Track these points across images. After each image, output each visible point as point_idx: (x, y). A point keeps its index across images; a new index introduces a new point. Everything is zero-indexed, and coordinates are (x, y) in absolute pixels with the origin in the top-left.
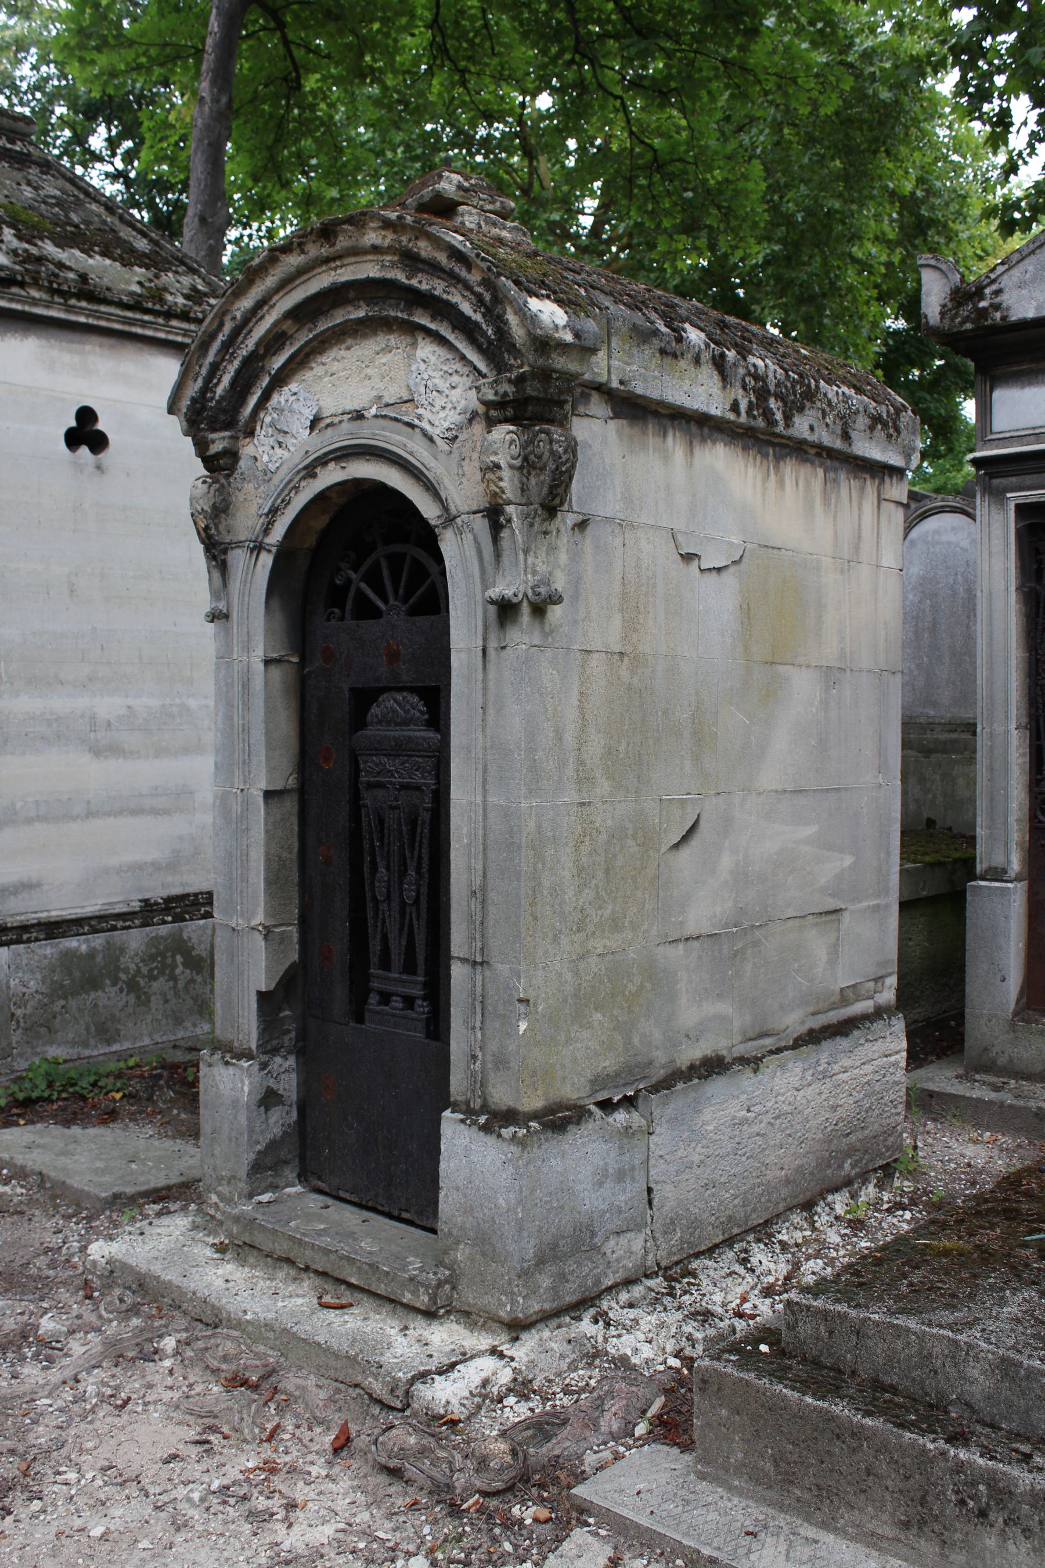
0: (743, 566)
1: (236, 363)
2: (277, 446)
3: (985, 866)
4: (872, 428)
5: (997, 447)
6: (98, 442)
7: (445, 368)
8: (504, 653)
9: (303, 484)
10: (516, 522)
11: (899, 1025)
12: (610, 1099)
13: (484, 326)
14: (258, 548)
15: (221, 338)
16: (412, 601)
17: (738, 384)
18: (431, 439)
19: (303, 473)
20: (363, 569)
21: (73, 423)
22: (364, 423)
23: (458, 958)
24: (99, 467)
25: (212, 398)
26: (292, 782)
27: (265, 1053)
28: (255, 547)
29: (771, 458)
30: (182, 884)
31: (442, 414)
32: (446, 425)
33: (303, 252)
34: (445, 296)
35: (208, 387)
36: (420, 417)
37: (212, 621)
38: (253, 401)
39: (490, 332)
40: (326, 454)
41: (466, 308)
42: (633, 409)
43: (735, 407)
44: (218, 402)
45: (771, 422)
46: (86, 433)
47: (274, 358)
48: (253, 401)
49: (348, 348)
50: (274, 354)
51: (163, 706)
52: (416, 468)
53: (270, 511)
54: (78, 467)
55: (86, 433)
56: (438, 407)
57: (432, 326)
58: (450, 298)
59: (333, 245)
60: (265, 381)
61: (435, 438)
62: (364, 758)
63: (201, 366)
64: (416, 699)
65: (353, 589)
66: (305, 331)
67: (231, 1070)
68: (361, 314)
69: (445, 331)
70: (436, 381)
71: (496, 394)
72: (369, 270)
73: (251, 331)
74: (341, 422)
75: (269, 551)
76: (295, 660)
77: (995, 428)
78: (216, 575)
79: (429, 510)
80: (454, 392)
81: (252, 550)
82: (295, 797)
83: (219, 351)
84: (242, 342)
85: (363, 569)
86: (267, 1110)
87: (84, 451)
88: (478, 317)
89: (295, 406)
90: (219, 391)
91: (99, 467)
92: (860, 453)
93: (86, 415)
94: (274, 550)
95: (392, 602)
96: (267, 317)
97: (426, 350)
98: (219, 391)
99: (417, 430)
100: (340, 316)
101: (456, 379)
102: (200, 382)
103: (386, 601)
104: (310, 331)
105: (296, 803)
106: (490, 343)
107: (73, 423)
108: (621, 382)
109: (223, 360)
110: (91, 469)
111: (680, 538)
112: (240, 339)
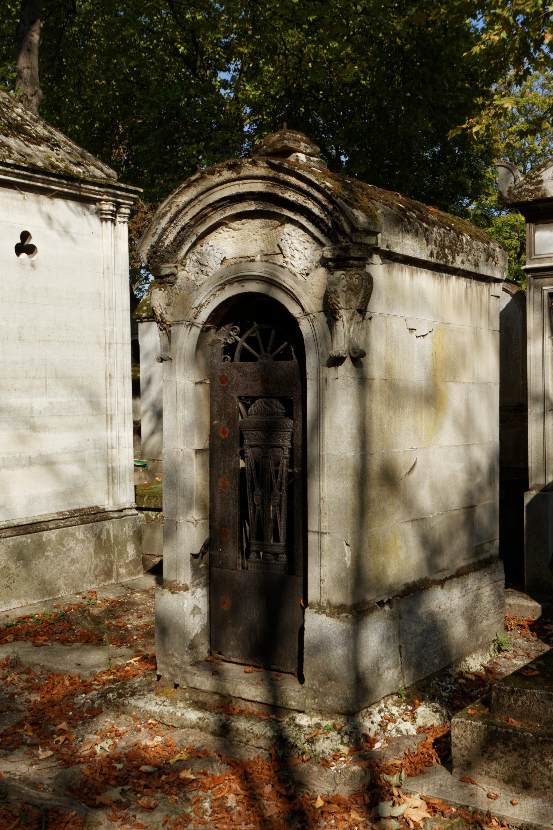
0: (433, 333)
1: (178, 229)
2: (200, 272)
3: (533, 483)
4: (487, 260)
5: (538, 263)
6: (31, 250)
7: (301, 239)
8: (337, 381)
9: (218, 293)
10: (344, 318)
11: (501, 565)
12: (382, 601)
13: (326, 221)
14: (192, 325)
15: (169, 215)
16: (275, 353)
17: (433, 243)
18: (295, 275)
19: (218, 288)
20: (245, 336)
21: (19, 241)
22: (255, 264)
23: (312, 531)
24: (33, 266)
25: (163, 246)
26: (207, 445)
27: (193, 586)
28: (189, 324)
29: (444, 278)
30: (78, 504)
31: (299, 262)
32: (302, 267)
33: (221, 175)
34: (304, 204)
35: (160, 240)
36: (286, 262)
37: (161, 362)
38: (186, 248)
39: (330, 224)
40: (233, 279)
41: (316, 210)
42: (391, 257)
43: (431, 255)
44: (166, 248)
45: (447, 261)
46: (25, 247)
47: (199, 227)
48: (186, 248)
49: (243, 224)
50: (199, 225)
51: (68, 402)
52: (287, 289)
53: (199, 306)
54: (21, 264)
55: (25, 247)
56: (297, 258)
57: (295, 218)
58: (307, 205)
59: (239, 173)
60: (194, 238)
61: (297, 274)
62: (247, 432)
63: (157, 229)
64: (278, 403)
65: (239, 346)
66: (219, 215)
67: (175, 595)
68: (253, 208)
69: (303, 220)
70: (296, 245)
71: (333, 255)
72: (258, 187)
73: (187, 213)
74: (241, 262)
75: (198, 327)
76: (208, 382)
77: (536, 253)
78: (166, 338)
79: (295, 310)
80: (306, 251)
81: (187, 326)
82: (208, 453)
83: (168, 222)
84: (182, 218)
85: (245, 336)
86: (194, 616)
87: (24, 255)
88: (322, 216)
89: (212, 252)
90: (167, 242)
91: (33, 266)
92: (482, 273)
93: (25, 235)
94: (201, 326)
95: (263, 352)
96: (197, 206)
97: (289, 228)
98: (167, 242)
99: (286, 269)
100: (240, 208)
101: (307, 245)
102: (156, 238)
103: (259, 353)
104: (222, 214)
105: (208, 456)
106: (329, 229)
107: (19, 241)
108: (387, 247)
109: (170, 226)
110: (28, 267)
111: (408, 321)
112: (180, 216)
